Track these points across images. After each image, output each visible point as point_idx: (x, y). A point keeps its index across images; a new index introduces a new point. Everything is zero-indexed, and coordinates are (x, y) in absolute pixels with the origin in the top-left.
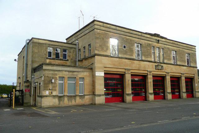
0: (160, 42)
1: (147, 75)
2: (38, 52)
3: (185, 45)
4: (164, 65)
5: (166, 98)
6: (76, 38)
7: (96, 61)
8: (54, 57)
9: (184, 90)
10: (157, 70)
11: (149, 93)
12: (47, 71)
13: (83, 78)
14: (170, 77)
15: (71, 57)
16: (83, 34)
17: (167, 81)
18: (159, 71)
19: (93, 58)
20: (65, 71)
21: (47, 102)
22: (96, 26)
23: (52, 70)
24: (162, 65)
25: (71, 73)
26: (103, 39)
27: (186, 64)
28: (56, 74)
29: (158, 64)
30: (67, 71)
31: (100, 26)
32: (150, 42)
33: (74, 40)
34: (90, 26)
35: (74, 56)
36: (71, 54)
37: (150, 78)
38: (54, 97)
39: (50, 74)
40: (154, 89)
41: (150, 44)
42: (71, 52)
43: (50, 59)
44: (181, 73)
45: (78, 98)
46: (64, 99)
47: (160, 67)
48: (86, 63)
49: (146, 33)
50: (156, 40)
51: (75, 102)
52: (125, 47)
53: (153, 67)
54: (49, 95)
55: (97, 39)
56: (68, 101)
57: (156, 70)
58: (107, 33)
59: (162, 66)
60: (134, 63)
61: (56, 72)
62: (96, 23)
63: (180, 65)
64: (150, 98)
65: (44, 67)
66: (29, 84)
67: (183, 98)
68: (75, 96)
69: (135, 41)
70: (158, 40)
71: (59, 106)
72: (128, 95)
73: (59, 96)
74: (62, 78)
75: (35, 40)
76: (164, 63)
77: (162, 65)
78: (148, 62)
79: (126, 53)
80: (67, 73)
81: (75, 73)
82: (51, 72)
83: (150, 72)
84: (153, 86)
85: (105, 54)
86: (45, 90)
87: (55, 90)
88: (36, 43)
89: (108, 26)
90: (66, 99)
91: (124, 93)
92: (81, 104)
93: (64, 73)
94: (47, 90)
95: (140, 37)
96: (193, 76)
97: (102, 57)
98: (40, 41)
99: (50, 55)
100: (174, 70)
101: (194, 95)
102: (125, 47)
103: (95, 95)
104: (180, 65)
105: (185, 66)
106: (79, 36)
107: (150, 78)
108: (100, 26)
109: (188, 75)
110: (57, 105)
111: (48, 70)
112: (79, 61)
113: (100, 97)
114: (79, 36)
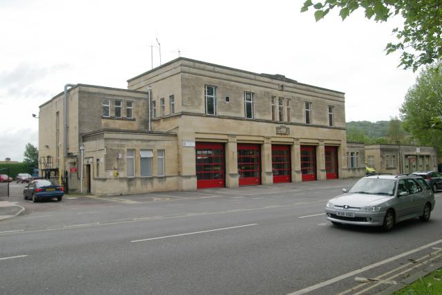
3: (225, 71)
25: (145, 143)
38: (121, 179)
61: (123, 143)
87: (123, 170)
98: (91, 90)
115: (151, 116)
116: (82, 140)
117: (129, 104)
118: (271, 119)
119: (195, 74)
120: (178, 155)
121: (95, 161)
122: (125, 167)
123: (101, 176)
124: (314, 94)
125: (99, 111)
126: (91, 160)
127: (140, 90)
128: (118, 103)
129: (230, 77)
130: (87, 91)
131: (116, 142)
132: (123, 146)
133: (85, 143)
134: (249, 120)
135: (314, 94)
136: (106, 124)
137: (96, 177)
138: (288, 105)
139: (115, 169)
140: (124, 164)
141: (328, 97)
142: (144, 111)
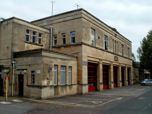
1: (110, 66)
2: (18, 33)
3: (127, 41)
5: (118, 86)
8: (31, 41)
9: (101, 81)
11: (111, 82)
12: (46, 57)
13: (71, 67)
14: (113, 66)
15: (45, 43)
17: (100, 70)
20: (59, 59)
21: (46, 93)
22: (83, 15)
23: (49, 57)
25: (63, 61)
28: (52, 62)
29: (116, 55)
30: (60, 59)
34: (72, 14)
35: (48, 41)
36: (45, 39)
38: (51, 86)
39: (47, 61)
44: (126, 64)
45: (68, 87)
49: (110, 27)
51: (66, 92)
54: (46, 85)
55: (83, 28)
56: (61, 91)
58: (89, 23)
61: (52, 60)
62: (83, 11)
64: (112, 86)
65: (43, 54)
67: (119, 87)
68: (66, 86)
71: (55, 97)
72: (101, 84)
73: (55, 86)
74: (56, 66)
75: (16, 21)
78: (111, 54)
80: (60, 61)
81: (66, 62)
85: (88, 44)
86: (44, 79)
87: (52, 80)
88: (17, 23)
89: (90, 16)
90: (60, 89)
91: (97, 82)
92: (70, 95)
94: (45, 79)
97: (87, 46)
98: (20, 22)
99: (28, 39)
101: (130, 83)
103: (82, 85)
110: (53, 96)
111: (46, 56)
113: (33, 88)
114: (54, 22)
115: (52, 43)
116: (13, 56)
117: (40, 35)
118: (122, 55)
119: (118, 38)
120: (78, 70)
121: (30, 73)
122: (53, 78)
123: (36, 84)
124: (124, 41)
125: (24, 37)
126: (25, 71)
127: (45, 27)
128: (34, 33)
129: (126, 42)
130: (18, 22)
131: (49, 59)
132: (52, 62)
133: (16, 59)
134: (32, 79)
135: (124, 41)
136: (28, 47)
137: (30, 83)
138: (122, 48)
139: (48, 79)
140: (52, 75)
141: (94, 22)
142: (48, 41)
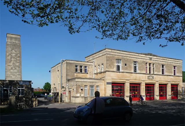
0: (152, 59)
4: (154, 76)
6: (93, 58)
7: (107, 75)
8: (79, 72)
10: (149, 80)
16: (98, 56)
18: (151, 80)
19: (105, 73)
24: (152, 76)
26: (111, 60)
27: (173, 74)
31: (110, 52)
32: (145, 60)
33: (91, 59)
37: (143, 85)
40: (160, 93)
41: (144, 61)
42: (89, 68)
43: (77, 73)
46: (87, 99)
47: (151, 78)
48: (103, 79)
50: (149, 58)
52: (126, 65)
53: (146, 78)
57: (148, 80)
59: (153, 77)
60: (132, 75)
63: (168, 76)
66: (65, 89)
69: (133, 60)
70: (151, 58)
76: (155, 75)
77: (152, 76)
79: (126, 69)
80: (89, 83)
81: (94, 83)
82: (80, 83)
83: (144, 81)
84: (159, 88)
93: (87, 83)
95: (137, 57)
96: (179, 83)
100: (162, 79)
102: (126, 65)
104: (168, 76)
105: (172, 76)
106: (95, 57)
107: (143, 85)
108: (110, 52)
109: (174, 82)
112: (95, 74)
